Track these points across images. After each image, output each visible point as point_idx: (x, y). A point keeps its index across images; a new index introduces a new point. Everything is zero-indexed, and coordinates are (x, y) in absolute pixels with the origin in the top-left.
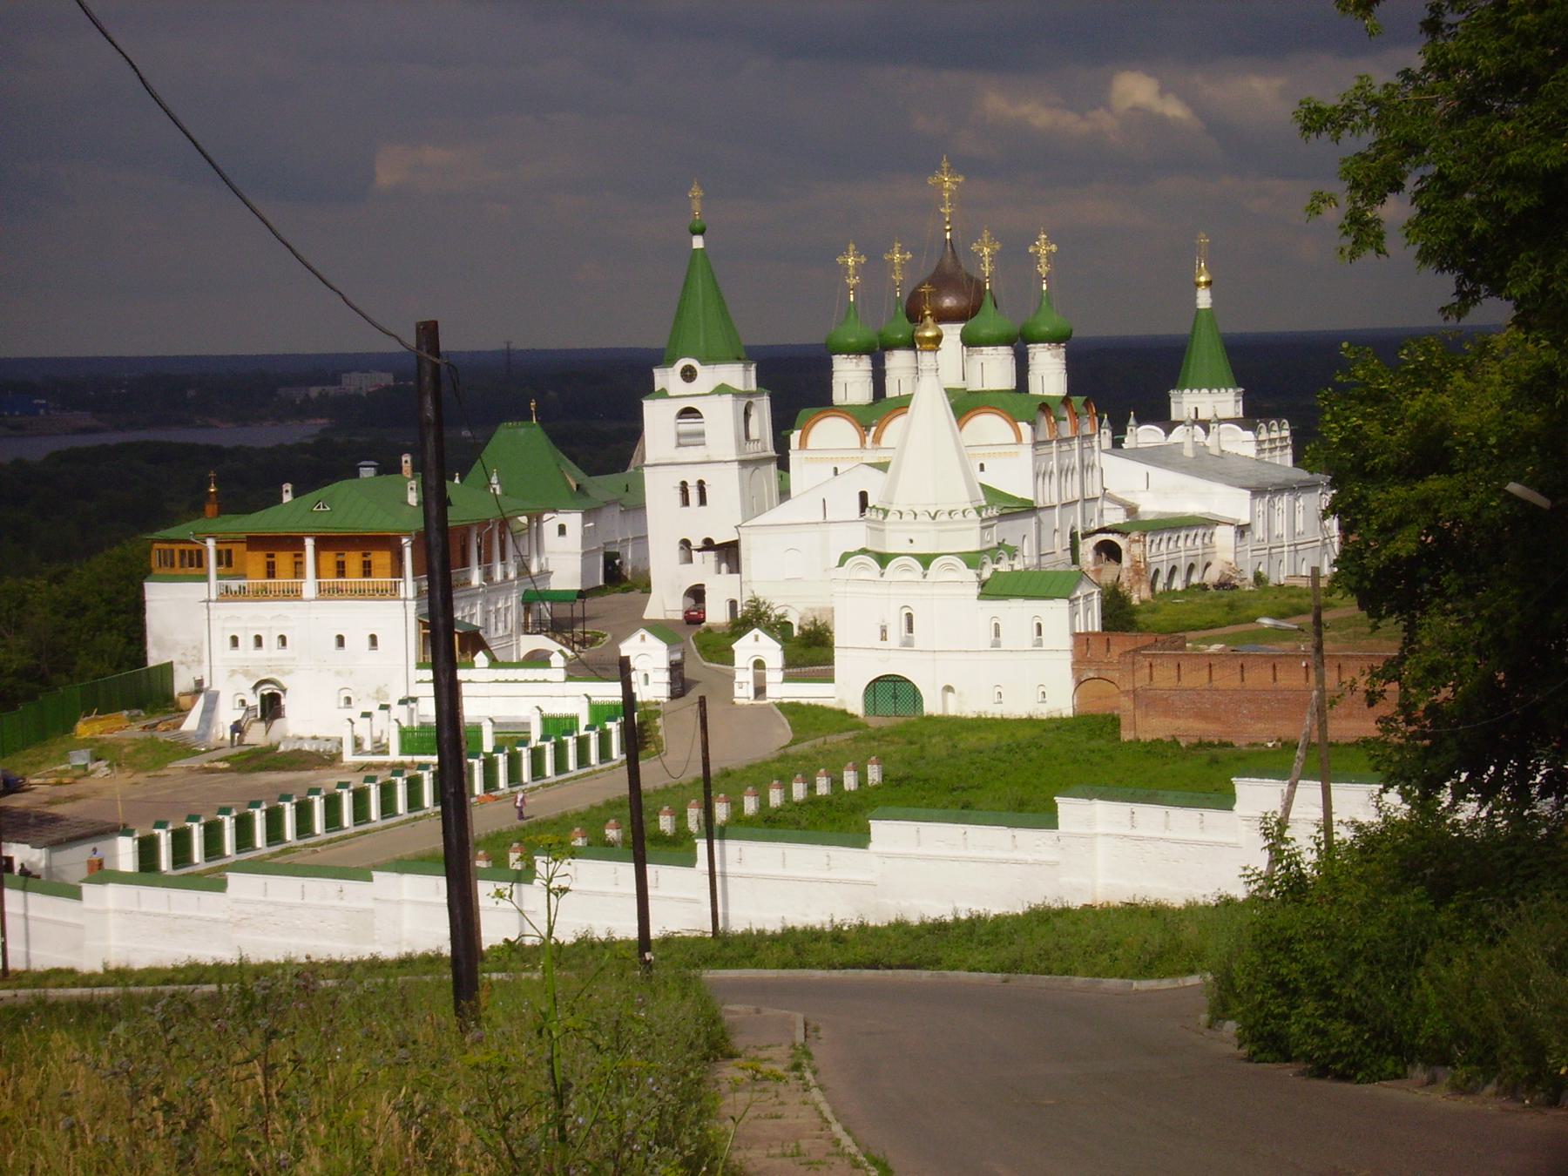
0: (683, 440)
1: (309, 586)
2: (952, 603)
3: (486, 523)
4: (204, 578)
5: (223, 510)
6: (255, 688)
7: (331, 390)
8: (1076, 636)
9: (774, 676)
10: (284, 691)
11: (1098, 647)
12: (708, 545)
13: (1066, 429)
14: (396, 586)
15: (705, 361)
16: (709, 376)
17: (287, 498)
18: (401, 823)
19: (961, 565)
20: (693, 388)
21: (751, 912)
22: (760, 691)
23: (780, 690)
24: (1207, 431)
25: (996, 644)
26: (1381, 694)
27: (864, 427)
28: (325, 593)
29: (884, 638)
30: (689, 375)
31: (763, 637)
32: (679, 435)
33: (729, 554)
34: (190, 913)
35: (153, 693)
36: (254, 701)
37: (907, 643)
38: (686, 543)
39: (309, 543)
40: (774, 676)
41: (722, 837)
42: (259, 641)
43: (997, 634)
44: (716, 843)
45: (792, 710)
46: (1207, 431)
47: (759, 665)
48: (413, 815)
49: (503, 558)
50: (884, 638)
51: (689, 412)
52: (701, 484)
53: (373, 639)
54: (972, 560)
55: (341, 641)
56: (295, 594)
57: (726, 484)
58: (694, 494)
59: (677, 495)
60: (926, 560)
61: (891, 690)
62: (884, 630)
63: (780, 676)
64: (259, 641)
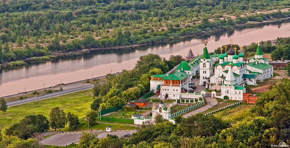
2: (232, 90)
9: (215, 95)
11: (245, 95)
14: (179, 85)
25: (240, 93)
27: (222, 67)
37: (228, 93)
39: (171, 81)
42: (166, 90)
47: (214, 95)
52: (205, 71)
54: (234, 85)
55: (174, 90)
56: (170, 86)
58: (205, 72)
61: (226, 97)
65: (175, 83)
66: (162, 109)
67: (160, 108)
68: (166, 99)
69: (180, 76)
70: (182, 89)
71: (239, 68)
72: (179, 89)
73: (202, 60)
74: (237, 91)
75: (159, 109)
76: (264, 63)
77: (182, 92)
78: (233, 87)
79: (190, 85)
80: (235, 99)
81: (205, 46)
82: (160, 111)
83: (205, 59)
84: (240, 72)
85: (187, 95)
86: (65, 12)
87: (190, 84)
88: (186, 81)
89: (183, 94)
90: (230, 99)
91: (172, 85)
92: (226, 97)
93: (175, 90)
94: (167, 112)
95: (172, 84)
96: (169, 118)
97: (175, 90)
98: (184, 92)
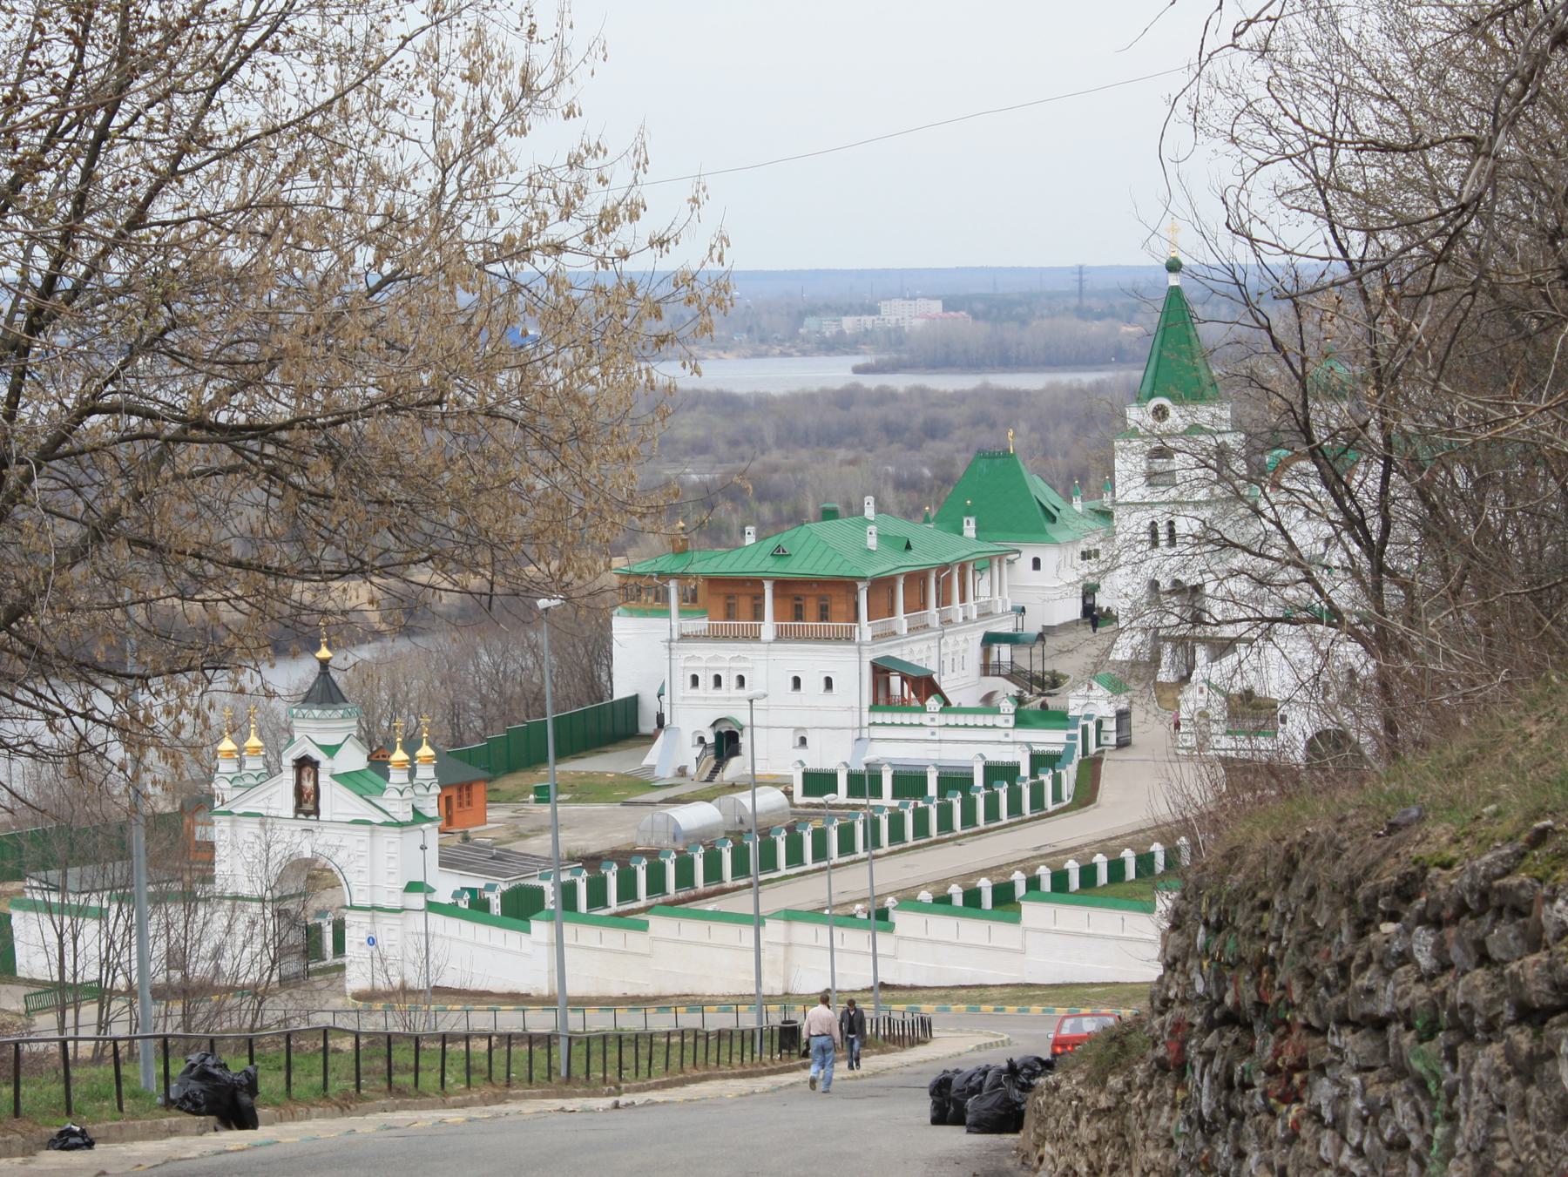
1: (768, 628)
3: (946, 566)
4: (665, 613)
5: (561, 755)
6: (714, 725)
7: (868, 321)
15: (1177, 400)
17: (750, 540)
18: (931, 844)
28: (781, 636)
36: (710, 739)
41: (53, 983)
42: (718, 681)
44: (56, 978)
48: (816, 866)
49: (963, 599)
53: (829, 683)
55: (797, 682)
56: (757, 638)
64: (718, 681)
65: (811, 606)
66: (323, 778)
67: (304, 764)
68: (709, 780)
69: (872, 542)
70: (881, 671)
72: (848, 665)
73: (1136, 415)
75: (289, 776)
77: (882, 699)
79: (1004, 652)
81: (1174, 280)
82: (307, 803)
85: (928, 731)
86: (1205, 1091)
87: (990, 640)
88: (944, 600)
89: (888, 718)
91: (779, 638)
93: (813, 683)
94: (378, 817)
95: (776, 619)
96: (412, 887)
97: (813, 683)
98: (904, 707)
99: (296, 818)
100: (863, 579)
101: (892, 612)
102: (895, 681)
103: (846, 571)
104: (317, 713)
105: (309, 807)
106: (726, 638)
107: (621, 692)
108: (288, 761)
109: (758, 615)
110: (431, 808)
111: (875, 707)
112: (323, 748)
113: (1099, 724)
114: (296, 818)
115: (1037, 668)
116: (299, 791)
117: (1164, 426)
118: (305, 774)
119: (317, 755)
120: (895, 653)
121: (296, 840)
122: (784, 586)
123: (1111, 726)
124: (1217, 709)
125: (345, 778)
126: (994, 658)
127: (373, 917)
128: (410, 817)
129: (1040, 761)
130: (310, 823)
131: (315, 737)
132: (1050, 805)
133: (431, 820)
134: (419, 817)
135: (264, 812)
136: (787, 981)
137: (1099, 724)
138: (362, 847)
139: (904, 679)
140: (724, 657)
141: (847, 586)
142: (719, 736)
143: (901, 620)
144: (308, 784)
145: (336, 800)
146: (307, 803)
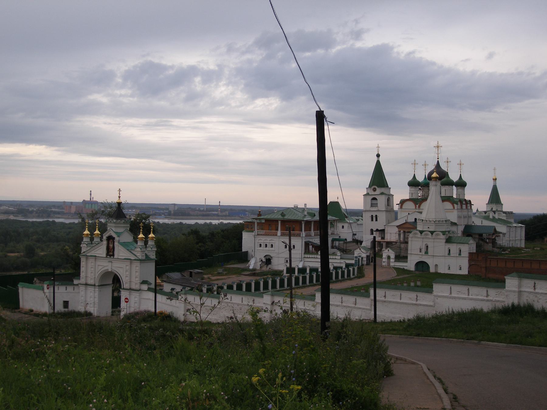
0: (372, 205)
1: (279, 233)
2: (438, 246)
6: (265, 257)
8: (470, 253)
9: (392, 260)
10: (272, 257)
12: (377, 230)
13: (464, 206)
15: (378, 187)
16: (379, 191)
19: (441, 234)
20: (376, 193)
21: (385, 314)
22: (389, 263)
23: (393, 263)
24: (495, 213)
25: (460, 254)
26: (56, 379)
27: (416, 204)
29: (420, 252)
30: (375, 190)
31: (390, 250)
32: (372, 204)
33: (383, 231)
34: (350, 305)
35: (245, 258)
36: (264, 260)
37: (426, 253)
38: (372, 230)
39: (279, 222)
40: (392, 260)
42: (266, 246)
43: (427, 249)
45: (397, 269)
46: (495, 213)
47: (389, 257)
50: (420, 252)
51: (374, 199)
52: (376, 216)
54: (444, 233)
56: (276, 235)
57: (382, 217)
59: (370, 219)
60: (432, 233)
61: (422, 266)
62: (421, 250)
63: (393, 261)
64: (266, 246)
66: (116, 244)
70: (307, 244)
71: (455, 205)
74: (454, 248)
75: (105, 243)
76: (505, 218)
78: (442, 236)
80: (447, 272)
82: (110, 252)
83: (375, 188)
84: (459, 217)
89: (308, 256)
90: (432, 270)
91: (282, 235)
92: (422, 266)
94: (133, 258)
95: (281, 230)
96: (144, 282)
98: (312, 253)
99: (106, 257)
100: (304, 221)
101: (310, 230)
102: (311, 247)
103: (300, 218)
104: (115, 221)
105: (111, 253)
106: (268, 235)
107: (244, 250)
108: (105, 238)
109: (277, 230)
110: (153, 256)
111: (304, 254)
112: (116, 233)
113: (362, 258)
114: (106, 257)
115: (345, 248)
116: (108, 248)
117: (376, 193)
118: (110, 242)
119: (114, 235)
120: (311, 240)
121: (106, 265)
122: (284, 222)
123: (365, 259)
124: (393, 256)
125: (124, 245)
126: (334, 245)
127: (130, 292)
128: (144, 258)
129: (347, 266)
130: (111, 259)
131: (114, 229)
132: (352, 276)
133: (151, 259)
134: (147, 259)
135: (97, 255)
136: (130, 286)
137: (362, 258)
138: (128, 268)
139: (313, 247)
140: (268, 240)
141: (299, 222)
142: (266, 259)
143: (313, 233)
144: (111, 246)
145: (120, 252)
146: (110, 252)
